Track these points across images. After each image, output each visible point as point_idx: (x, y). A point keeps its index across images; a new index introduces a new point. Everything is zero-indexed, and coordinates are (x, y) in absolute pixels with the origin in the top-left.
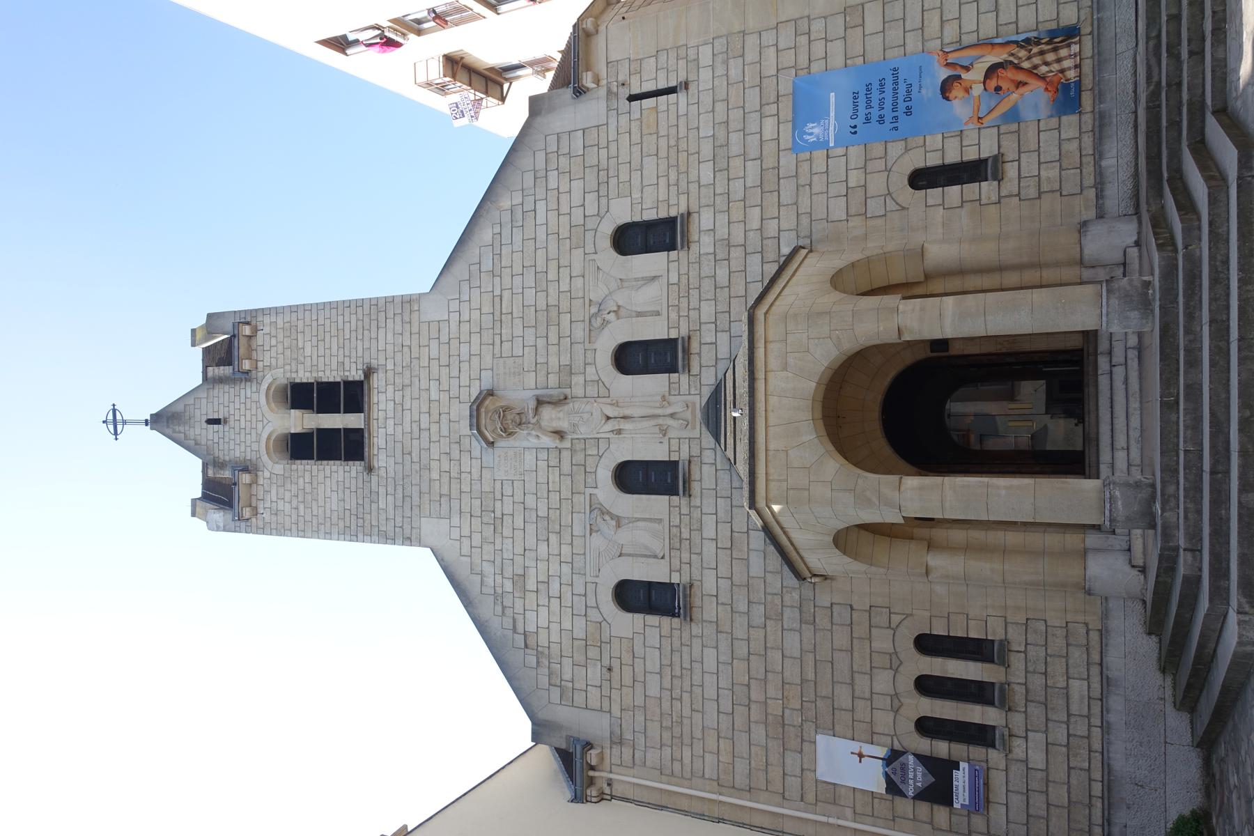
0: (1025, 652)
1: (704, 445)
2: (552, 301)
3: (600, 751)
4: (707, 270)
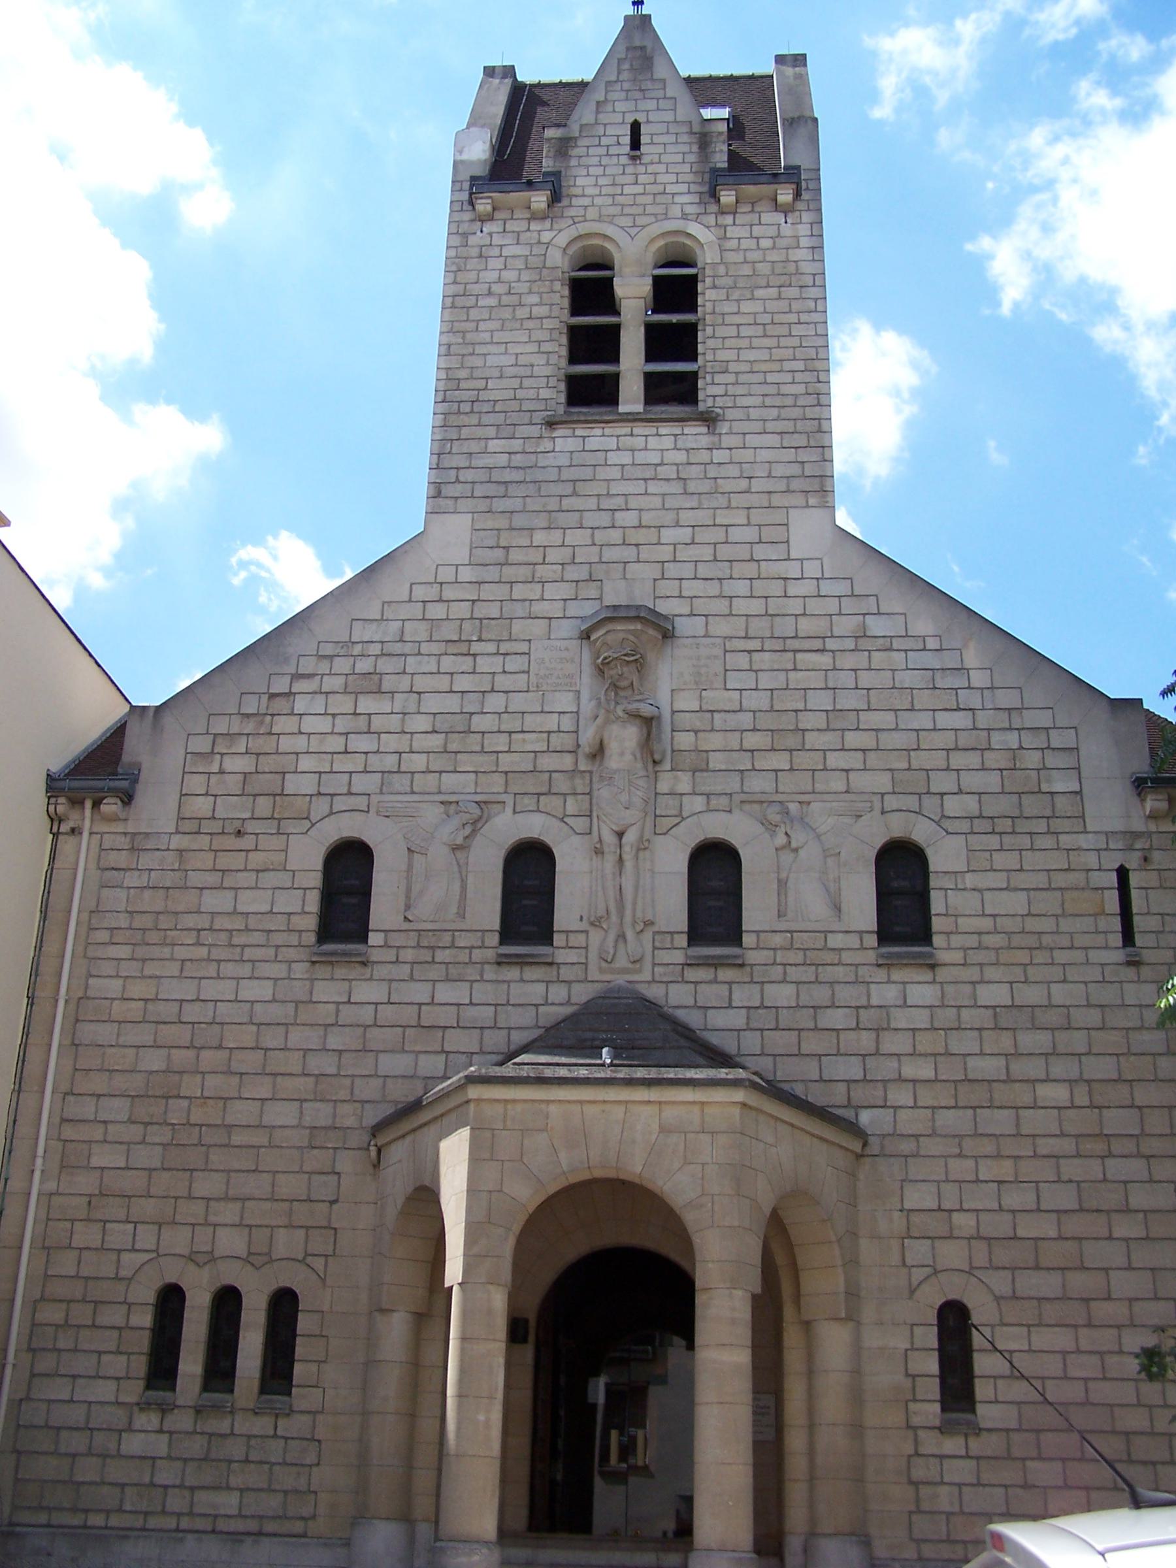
0: (275, 1436)
1: (576, 988)
2: (812, 739)
3: (121, 817)
4: (845, 994)
